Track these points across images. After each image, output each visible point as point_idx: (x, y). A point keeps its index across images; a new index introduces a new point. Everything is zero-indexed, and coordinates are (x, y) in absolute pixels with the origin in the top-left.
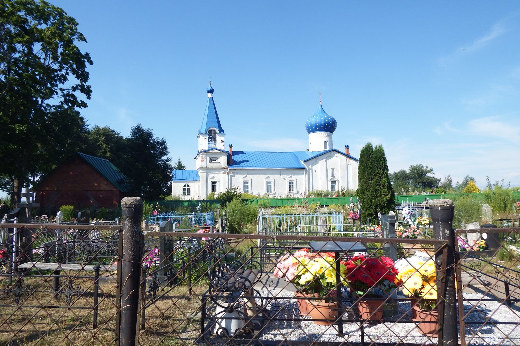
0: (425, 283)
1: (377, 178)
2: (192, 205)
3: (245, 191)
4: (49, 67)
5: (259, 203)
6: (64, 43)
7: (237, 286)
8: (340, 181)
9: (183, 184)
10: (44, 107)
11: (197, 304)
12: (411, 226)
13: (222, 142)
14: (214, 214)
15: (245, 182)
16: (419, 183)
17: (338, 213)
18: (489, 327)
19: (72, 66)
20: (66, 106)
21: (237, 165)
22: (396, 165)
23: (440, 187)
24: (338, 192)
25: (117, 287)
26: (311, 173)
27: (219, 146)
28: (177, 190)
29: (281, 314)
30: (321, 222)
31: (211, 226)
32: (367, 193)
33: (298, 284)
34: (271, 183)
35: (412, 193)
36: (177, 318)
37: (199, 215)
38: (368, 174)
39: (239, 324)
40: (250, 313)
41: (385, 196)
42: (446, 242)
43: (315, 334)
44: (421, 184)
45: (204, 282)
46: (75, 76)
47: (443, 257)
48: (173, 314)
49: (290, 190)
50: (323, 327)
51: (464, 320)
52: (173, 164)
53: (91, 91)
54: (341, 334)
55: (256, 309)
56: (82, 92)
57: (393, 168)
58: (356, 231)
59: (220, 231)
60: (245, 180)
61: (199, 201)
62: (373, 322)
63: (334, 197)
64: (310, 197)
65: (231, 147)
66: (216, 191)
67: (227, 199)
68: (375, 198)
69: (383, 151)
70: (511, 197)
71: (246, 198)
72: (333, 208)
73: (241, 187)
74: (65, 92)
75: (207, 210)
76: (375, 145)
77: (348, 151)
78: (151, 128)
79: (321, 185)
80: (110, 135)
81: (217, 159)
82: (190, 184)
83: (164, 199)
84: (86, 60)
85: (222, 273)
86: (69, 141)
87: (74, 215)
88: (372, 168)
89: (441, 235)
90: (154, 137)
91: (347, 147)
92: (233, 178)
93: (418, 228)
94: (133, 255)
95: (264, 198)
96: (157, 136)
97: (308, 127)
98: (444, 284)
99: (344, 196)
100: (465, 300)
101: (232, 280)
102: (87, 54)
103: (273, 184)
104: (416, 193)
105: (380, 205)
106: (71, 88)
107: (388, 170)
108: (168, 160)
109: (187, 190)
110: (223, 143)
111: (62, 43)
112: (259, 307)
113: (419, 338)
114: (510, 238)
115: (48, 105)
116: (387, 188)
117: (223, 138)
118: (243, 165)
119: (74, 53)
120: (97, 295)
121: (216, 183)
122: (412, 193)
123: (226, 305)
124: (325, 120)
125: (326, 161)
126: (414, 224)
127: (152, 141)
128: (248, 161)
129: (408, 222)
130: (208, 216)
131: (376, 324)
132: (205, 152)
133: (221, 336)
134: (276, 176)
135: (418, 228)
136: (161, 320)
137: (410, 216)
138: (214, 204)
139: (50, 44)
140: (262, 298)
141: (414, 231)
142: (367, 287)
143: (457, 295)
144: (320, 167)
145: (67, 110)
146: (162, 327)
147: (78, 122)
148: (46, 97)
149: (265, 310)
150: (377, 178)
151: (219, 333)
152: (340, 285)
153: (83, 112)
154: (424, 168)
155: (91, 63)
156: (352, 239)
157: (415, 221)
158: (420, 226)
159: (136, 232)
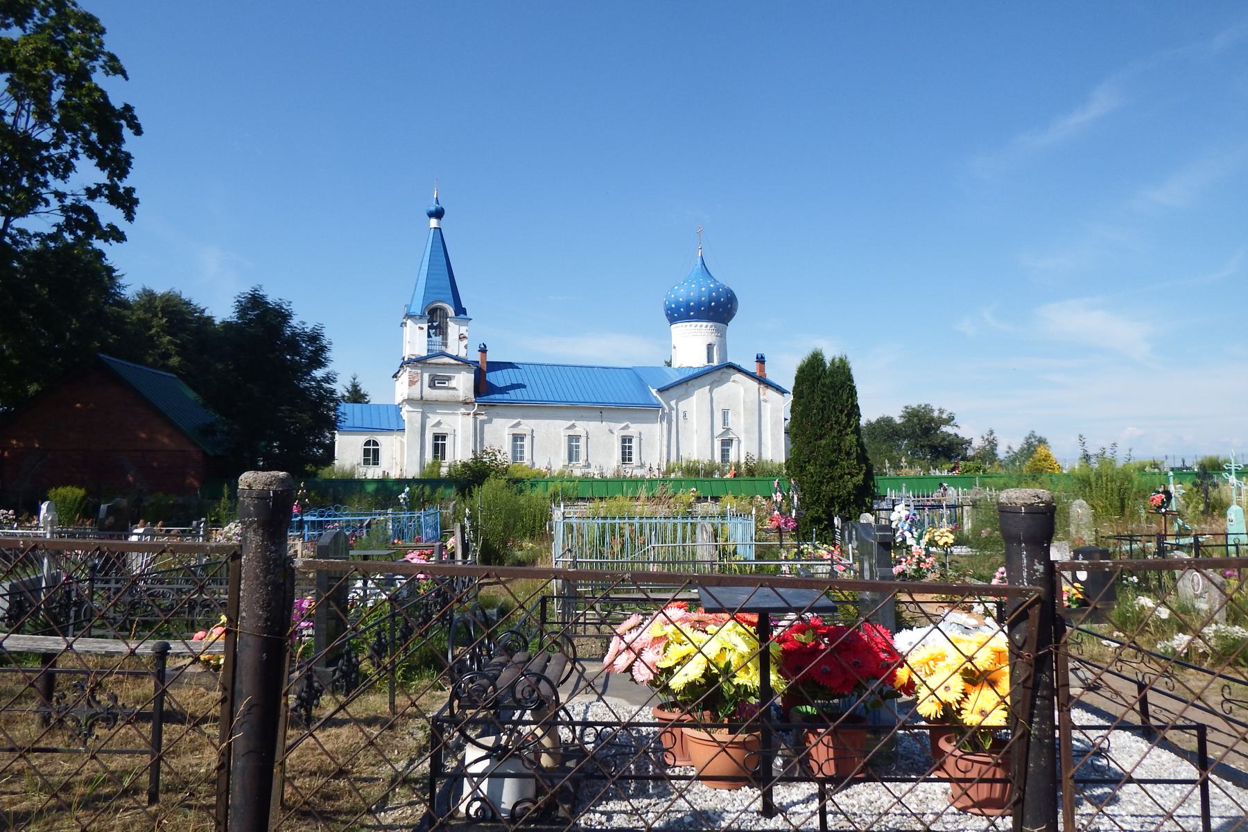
0: (970, 688)
1: (834, 433)
2: (386, 491)
3: (515, 458)
4: (27, 137)
5: (551, 489)
6: (67, 78)
7: (519, 696)
8: (742, 438)
9: (363, 439)
10: (12, 237)
11: (416, 734)
12: (913, 549)
13: (462, 337)
14: (441, 514)
15: (517, 438)
16: (922, 447)
17: (742, 514)
18: (1107, 790)
19: (86, 135)
20: (69, 237)
21: (498, 396)
22: (878, 402)
23: (973, 459)
24: (738, 465)
25: (223, 701)
26: (674, 418)
27: (455, 347)
28: (347, 451)
29: (622, 763)
30: (703, 538)
31: (431, 548)
32: (811, 468)
33: (666, 689)
34: (578, 440)
35: (906, 471)
36: (364, 775)
37: (404, 516)
38: (813, 424)
39: (521, 790)
40: (545, 761)
41: (852, 476)
42: (1036, 591)
43: (705, 812)
44: (927, 450)
45: (426, 682)
46: (95, 161)
47: (1030, 627)
48: (353, 765)
49: (624, 459)
50: (724, 793)
51: (1072, 777)
52: (340, 388)
53: (136, 202)
54: (769, 810)
55: (564, 752)
56: (112, 203)
57: (869, 413)
58: (786, 559)
59: (459, 556)
60: (517, 431)
61: (402, 482)
62: (842, 780)
63: (728, 476)
64: (673, 476)
65: (483, 351)
66: (443, 457)
67: (473, 476)
68: (828, 482)
69: (849, 370)
70: (1136, 483)
71: (518, 475)
72: (730, 504)
73: (507, 448)
74: (68, 201)
75: (423, 503)
76: (830, 355)
77: (762, 370)
78: (286, 298)
79: (698, 448)
80: (181, 313)
81: (449, 379)
82: (380, 439)
83: (315, 474)
84: (123, 122)
85: (479, 662)
86: (75, 324)
87: (87, 510)
88: (823, 409)
89: (1025, 574)
90: (294, 322)
91: (761, 360)
92: (486, 427)
93: (928, 554)
94: (267, 620)
95: (561, 477)
96: (303, 318)
97: (671, 309)
98: (1029, 692)
99: (753, 475)
100: (1075, 727)
101: (506, 676)
102: (128, 108)
103: (527, 442)
104: (917, 471)
105: (839, 497)
106: (83, 192)
107: (860, 415)
108: (328, 379)
109: (372, 455)
110: (465, 342)
111: (62, 78)
112: (566, 745)
113: (950, 818)
114: (1135, 579)
115: (22, 232)
116: (857, 457)
117: (463, 330)
118: (512, 395)
119: (95, 104)
120: (162, 715)
121: (444, 438)
122: (906, 471)
123: (489, 741)
124: (710, 295)
125: (711, 391)
126: (918, 544)
127: (288, 332)
128: (524, 386)
129: (904, 540)
130: (427, 517)
131: (848, 786)
132: (419, 361)
133: (478, 820)
134: (591, 423)
135: (928, 554)
136: (321, 781)
137: (911, 526)
138: (440, 490)
139: (30, 77)
140: (571, 724)
141: (920, 561)
142: (825, 696)
143: (1056, 713)
144: (695, 404)
145: (72, 246)
146: (327, 797)
147: (100, 277)
148: (18, 211)
149: (580, 753)
150: (834, 433)
151: (472, 811)
152: (766, 690)
153: (113, 253)
154: (936, 414)
155: (138, 131)
156: (774, 581)
157: (920, 537)
158: (932, 549)
159: (275, 560)
